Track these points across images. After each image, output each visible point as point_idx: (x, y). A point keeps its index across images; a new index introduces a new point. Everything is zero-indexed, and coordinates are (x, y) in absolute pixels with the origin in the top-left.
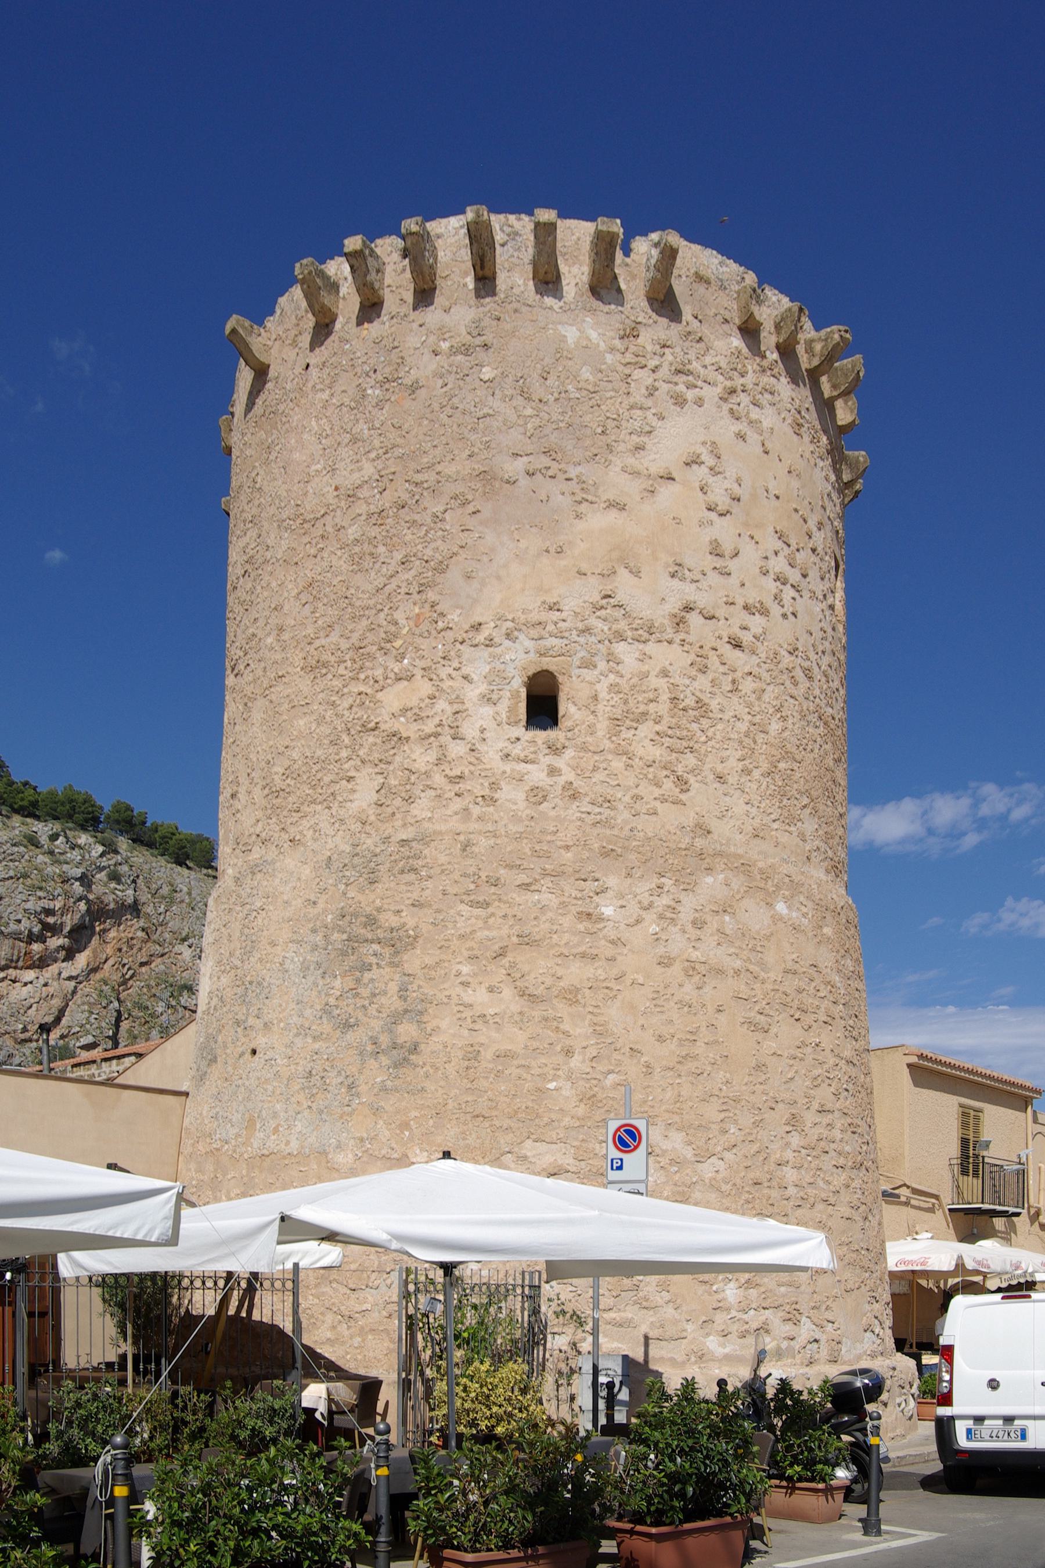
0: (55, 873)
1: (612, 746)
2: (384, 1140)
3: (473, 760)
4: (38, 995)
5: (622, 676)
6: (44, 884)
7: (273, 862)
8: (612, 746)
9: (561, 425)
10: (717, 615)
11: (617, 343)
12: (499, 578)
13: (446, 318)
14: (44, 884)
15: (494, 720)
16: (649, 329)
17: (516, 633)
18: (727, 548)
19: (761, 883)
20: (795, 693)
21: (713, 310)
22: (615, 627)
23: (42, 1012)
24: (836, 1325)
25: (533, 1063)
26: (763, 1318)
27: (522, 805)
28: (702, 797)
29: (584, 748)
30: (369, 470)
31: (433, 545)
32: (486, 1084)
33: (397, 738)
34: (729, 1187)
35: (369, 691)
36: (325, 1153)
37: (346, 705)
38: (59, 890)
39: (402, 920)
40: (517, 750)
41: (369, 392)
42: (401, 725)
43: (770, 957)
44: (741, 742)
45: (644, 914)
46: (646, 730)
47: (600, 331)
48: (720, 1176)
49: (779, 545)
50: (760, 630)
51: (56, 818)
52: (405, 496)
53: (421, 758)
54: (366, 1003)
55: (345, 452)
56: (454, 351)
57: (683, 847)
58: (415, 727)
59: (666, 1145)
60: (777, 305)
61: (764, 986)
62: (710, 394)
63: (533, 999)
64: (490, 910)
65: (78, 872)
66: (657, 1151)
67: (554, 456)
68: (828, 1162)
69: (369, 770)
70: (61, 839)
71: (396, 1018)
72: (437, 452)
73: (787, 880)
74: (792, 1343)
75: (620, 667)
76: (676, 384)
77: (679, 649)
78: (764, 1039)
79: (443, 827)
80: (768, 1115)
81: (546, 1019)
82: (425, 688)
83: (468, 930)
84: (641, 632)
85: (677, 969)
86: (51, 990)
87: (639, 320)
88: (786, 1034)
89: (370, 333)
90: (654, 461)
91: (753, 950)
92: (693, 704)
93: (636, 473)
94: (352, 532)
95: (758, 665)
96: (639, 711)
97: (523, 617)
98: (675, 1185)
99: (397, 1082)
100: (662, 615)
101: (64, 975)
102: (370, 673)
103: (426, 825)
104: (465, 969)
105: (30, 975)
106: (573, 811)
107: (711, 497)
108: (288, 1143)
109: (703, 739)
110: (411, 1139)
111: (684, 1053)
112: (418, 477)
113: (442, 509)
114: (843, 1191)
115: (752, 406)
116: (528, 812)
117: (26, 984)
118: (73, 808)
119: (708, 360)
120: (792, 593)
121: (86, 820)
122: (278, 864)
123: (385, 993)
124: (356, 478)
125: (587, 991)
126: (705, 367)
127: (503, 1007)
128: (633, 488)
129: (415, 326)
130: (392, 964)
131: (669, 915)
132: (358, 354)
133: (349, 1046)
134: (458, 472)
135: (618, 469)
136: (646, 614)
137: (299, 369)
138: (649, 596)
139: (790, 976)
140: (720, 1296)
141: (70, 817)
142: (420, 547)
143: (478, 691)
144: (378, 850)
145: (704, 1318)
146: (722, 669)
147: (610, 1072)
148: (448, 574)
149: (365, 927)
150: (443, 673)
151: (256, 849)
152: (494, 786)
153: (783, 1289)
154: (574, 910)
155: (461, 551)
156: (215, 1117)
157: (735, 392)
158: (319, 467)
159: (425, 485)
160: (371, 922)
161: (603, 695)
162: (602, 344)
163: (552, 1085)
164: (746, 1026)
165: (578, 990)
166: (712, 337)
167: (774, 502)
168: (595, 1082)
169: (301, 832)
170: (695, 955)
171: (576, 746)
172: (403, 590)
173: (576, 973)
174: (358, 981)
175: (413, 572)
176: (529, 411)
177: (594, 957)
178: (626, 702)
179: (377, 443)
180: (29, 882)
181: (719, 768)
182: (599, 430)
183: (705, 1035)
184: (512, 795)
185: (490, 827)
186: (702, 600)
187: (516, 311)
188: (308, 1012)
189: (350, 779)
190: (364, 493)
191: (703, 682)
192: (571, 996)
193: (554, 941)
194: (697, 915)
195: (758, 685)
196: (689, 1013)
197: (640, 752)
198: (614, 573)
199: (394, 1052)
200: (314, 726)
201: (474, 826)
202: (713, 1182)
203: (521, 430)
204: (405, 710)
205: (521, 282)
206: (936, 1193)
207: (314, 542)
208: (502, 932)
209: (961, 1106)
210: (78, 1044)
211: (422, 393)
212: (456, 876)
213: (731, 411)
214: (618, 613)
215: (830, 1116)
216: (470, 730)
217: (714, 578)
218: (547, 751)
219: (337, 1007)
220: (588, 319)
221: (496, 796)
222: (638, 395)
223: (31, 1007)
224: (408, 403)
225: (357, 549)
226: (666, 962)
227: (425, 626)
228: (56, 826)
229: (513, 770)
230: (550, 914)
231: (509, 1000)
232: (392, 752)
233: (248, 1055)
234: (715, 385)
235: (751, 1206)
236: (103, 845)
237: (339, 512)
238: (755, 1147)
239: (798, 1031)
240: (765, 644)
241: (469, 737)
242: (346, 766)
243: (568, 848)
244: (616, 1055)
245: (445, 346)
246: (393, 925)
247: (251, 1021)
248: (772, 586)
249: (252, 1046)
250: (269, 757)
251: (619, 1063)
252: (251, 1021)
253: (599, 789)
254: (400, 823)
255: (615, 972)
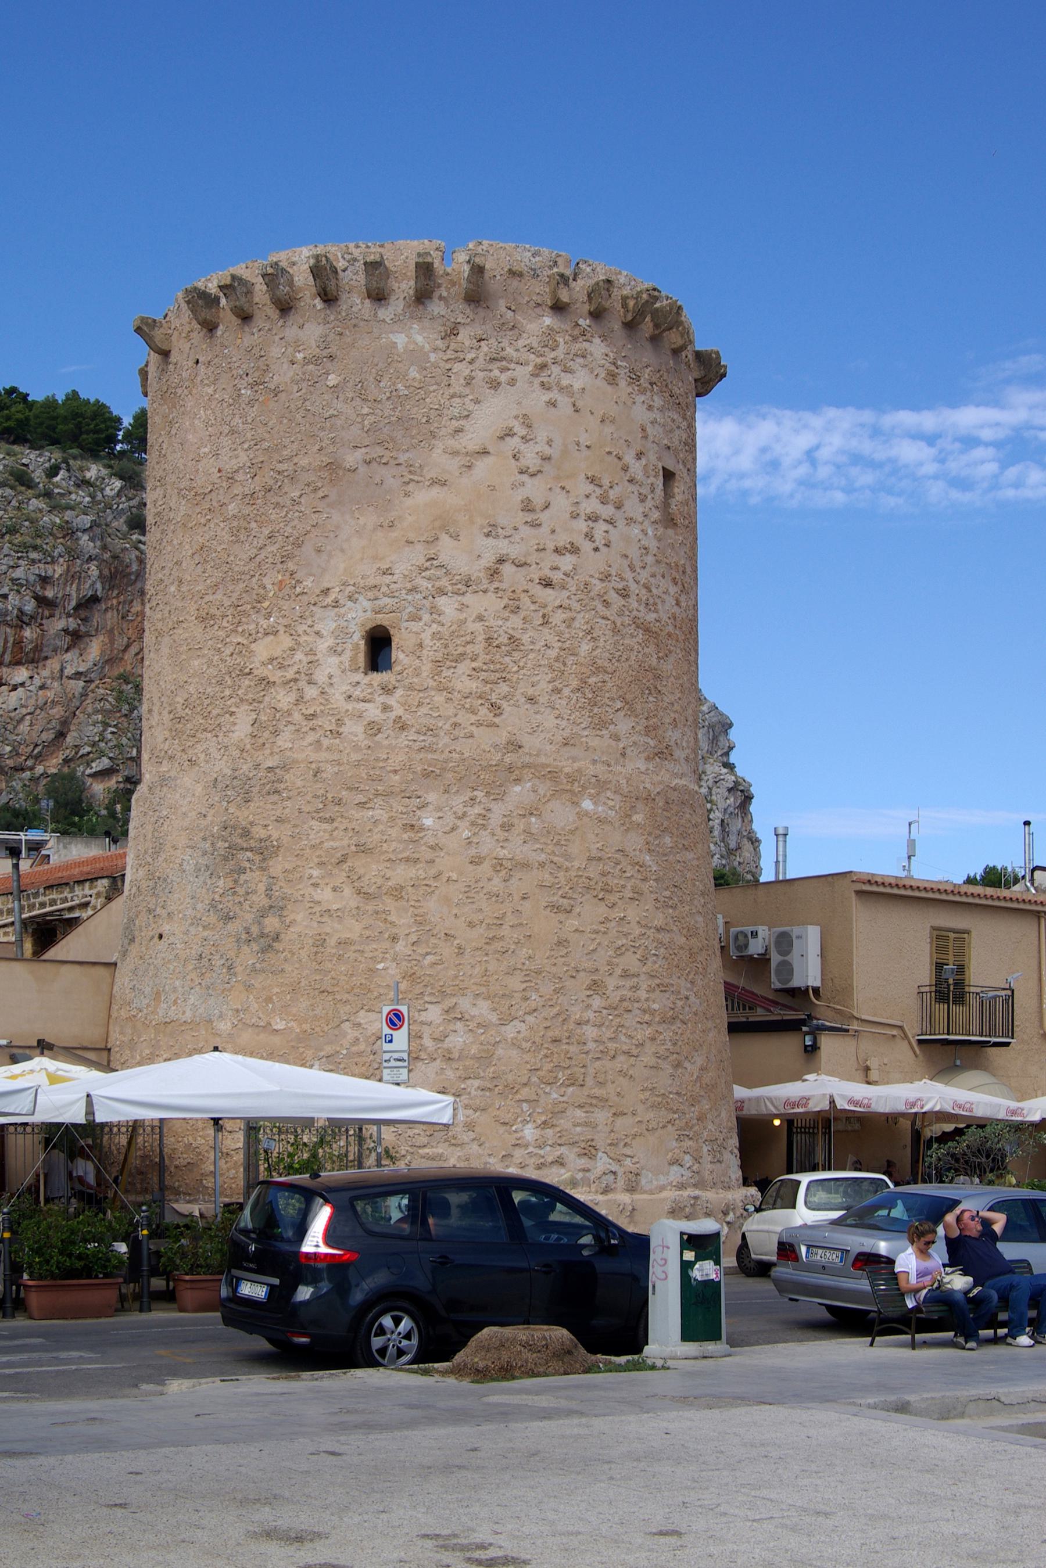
0: (54, 524)
1: (435, 684)
2: (254, 1011)
3: (323, 701)
4: (32, 702)
5: (443, 625)
6: (39, 541)
7: (175, 779)
8: (435, 684)
9: (393, 419)
10: (528, 562)
11: (440, 343)
12: (342, 550)
13: (300, 333)
14: (39, 541)
15: (338, 665)
16: (467, 327)
17: (357, 596)
18: (538, 501)
19: (567, 786)
20: (607, 613)
21: (527, 298)
22: (437, 584)
23: (38, 728)
24: (635, 1160)
25: (367, 948)
26: (558, 1153)
27: (361, 736)
28: (514, 719)
29: (411, 688)
30: (243, 458)
31: (293, 524)
32: (330, 966)
33: (266, 683)
34: (529, 1044)
35: (245, 642)
36: (210, 1021)
37: (228, 652)
38: (60, 549)
39: (269, 833)
40: (357, 693)
41: (243, 392)
42: (268, 671)
43: (574, 849)
44: (551, 667)
45: (458, 823)
46: (465, 667)
47: (425, 335)
48: (521, 1036)
49: (590, 488)
50: (571, 567)
51: (54, 442)
52: (271, 482)
53: (284, 699)
54: (242, 899)
55: (226, 441)
56: (306, 361)
57: (494, 763)
58: (279, 673)
59: (474, 1012)
60: (591, 275)
61: (568, 874)
62: (522, 372)
63: (367, 896)
64: (335, 824)
65: (86, 520)
66: (467, 1017)
67: (387, 445)
68: (630, 1020)
69: (245, 707)
70: (62, 473)
71: (263, 913)
72: (295, 446)
73: (594, 780)
74: (587, 1174)
75: (441, 618)
76: (491, 371)
77: (493, 596)
78: (567, 918)
79: (300, 756)
80: (569, 983)
81: (377, 913)
82: (287, 642)
83: (318, 841)
84: (459, 586)
85: (486, 867)
86: (50, 694)
87: (458, 320)
88: (590, 911)
89: (243, 342)
90: (470, 441)
91: (558, 844)
92: (506, 641)
93: (455, 453)
94: (232, 508)
95: (569, 598)
96: (458, 652)
97: (362, 582)
98: (481, 1044)
99: (264, 965)
100: (477, 569)
101: (69, 671)
102: (246, 627)
103: (288, 753)
104: (315, 873)
105: (21, 674)
106: (403, 740)
107: (524, 462)
108: (184, 1013)
109: (516, 669)
110: (273, 1010)
111: (491, 936)
112: (281, 467)
113: (298, 494)
114: (648, 1043)
115: (563, 374)
116: (366, 742)
117: (15, 688)
118: (79, 426)
119: (521, 343)
120: (605, 526)
121: (97, 443)
122: (178, 781)
123: (255, 892)
124: (234, 464)
125: (410, 888)
126: (517, 350)
127: (344, 903)
128: (453, 465)
129: (277, 338)
130: (263, 869)
131: (480, 822)
132: (234, 359)
133: (229, 935)
134: (310, 464)
135: (440, 451)
136: (465, 570)
137: (191, 363)
138: (463, 556)
139: (594, 863)
140: (518, 1135)
141: (74, 439)
142: (282, 525)
143: (327, 644)
144: (251, 775)
145: (504, 1153)
146: (533, 607)
147: (427, 954)
148: (303, 549)
149: (241, 837)
150: (301, 629)
151: (165, 762)
152: (340, 722)
153: (578, 1129)
154: (400, 823)
155: (313, 530)
156: (133, 989)
157: (546, 366)
158: (206, 450)
159: (286, 474)
160: (246, 833)
161: (428, 642)
162: (427, 346)
163: (380, 966)
164: (549, 909)
165: (402, 888)
166: (525, 322)
167: (585, 452)
168: (414, 962)
169: (196, 754)
170: (503, 853)
171: (405, 686)
172: (270, 560)
173: (401, 874)
174: (236, 881)
175: (277, 546)
176: (366, 410)
177: (416, 861)
178: (446, 646)
179: (249, 435)
180: (18, 539)
181: (530, 691)
182: (424, 420)
183: (511, 920)
184: (354, 729)
185: (336, 757)
186: (514, 551)
187: (355, 326)
188: (199, 906)
189: (232, 714)
190: (240, 477)
191: (516, 621)
192: (397, 893)
193: (384, 849)
194: (505, 820)
195: (568, 615)
196: (496, 901)
197: (459, 686)
198: (437, 539)
199: (262, 940)
200: (205, 667)
201: (323, 755)
202: (515, 1041)
203: (360, 426)
204: (271, 660)
205: (358, 302)
206: (899, 1023)
207: (204, 512)
208: (343, 842)
209: (934, 928)
210: (88, 771)
211: (283, 396)
212: (309, 797)
213: (542, 384)
214: (440, 573)
215: (635, 980)
216: (321, 676)
217: (526, 531)
218: (381, 692)
219: (221, 902)
220: (415, 326)
221: (341, 730)
222: (457, 386)
223: (22, 719)
224: (272, 404)
225: (235, 524)
226: (477, 861)
227: (287, 591)
228: (55, 455)
229: (354, 708)
230: (381, 827)
231: (349, 898)
232: (262, 693)
233: (156, 939)
234: (527, 364)
235: (548, 1060)
236: (121, 478)
237: (221, 491)
238: (555, 1010)
239: (602, 910)
240: (576, 578)
241: (320, 682)
242: (229, 703)
243: (395, 771)
244: (433, 940)
245: (300, 356)
246: (262, 837)
247: (159, 911)
248: (582, 525)
249: (159, 931)
250: (173, 688)
251: (435, 946)
252: (159, 911)
253: (423, 721)
254: (268, 752)
255: (433, 872)
